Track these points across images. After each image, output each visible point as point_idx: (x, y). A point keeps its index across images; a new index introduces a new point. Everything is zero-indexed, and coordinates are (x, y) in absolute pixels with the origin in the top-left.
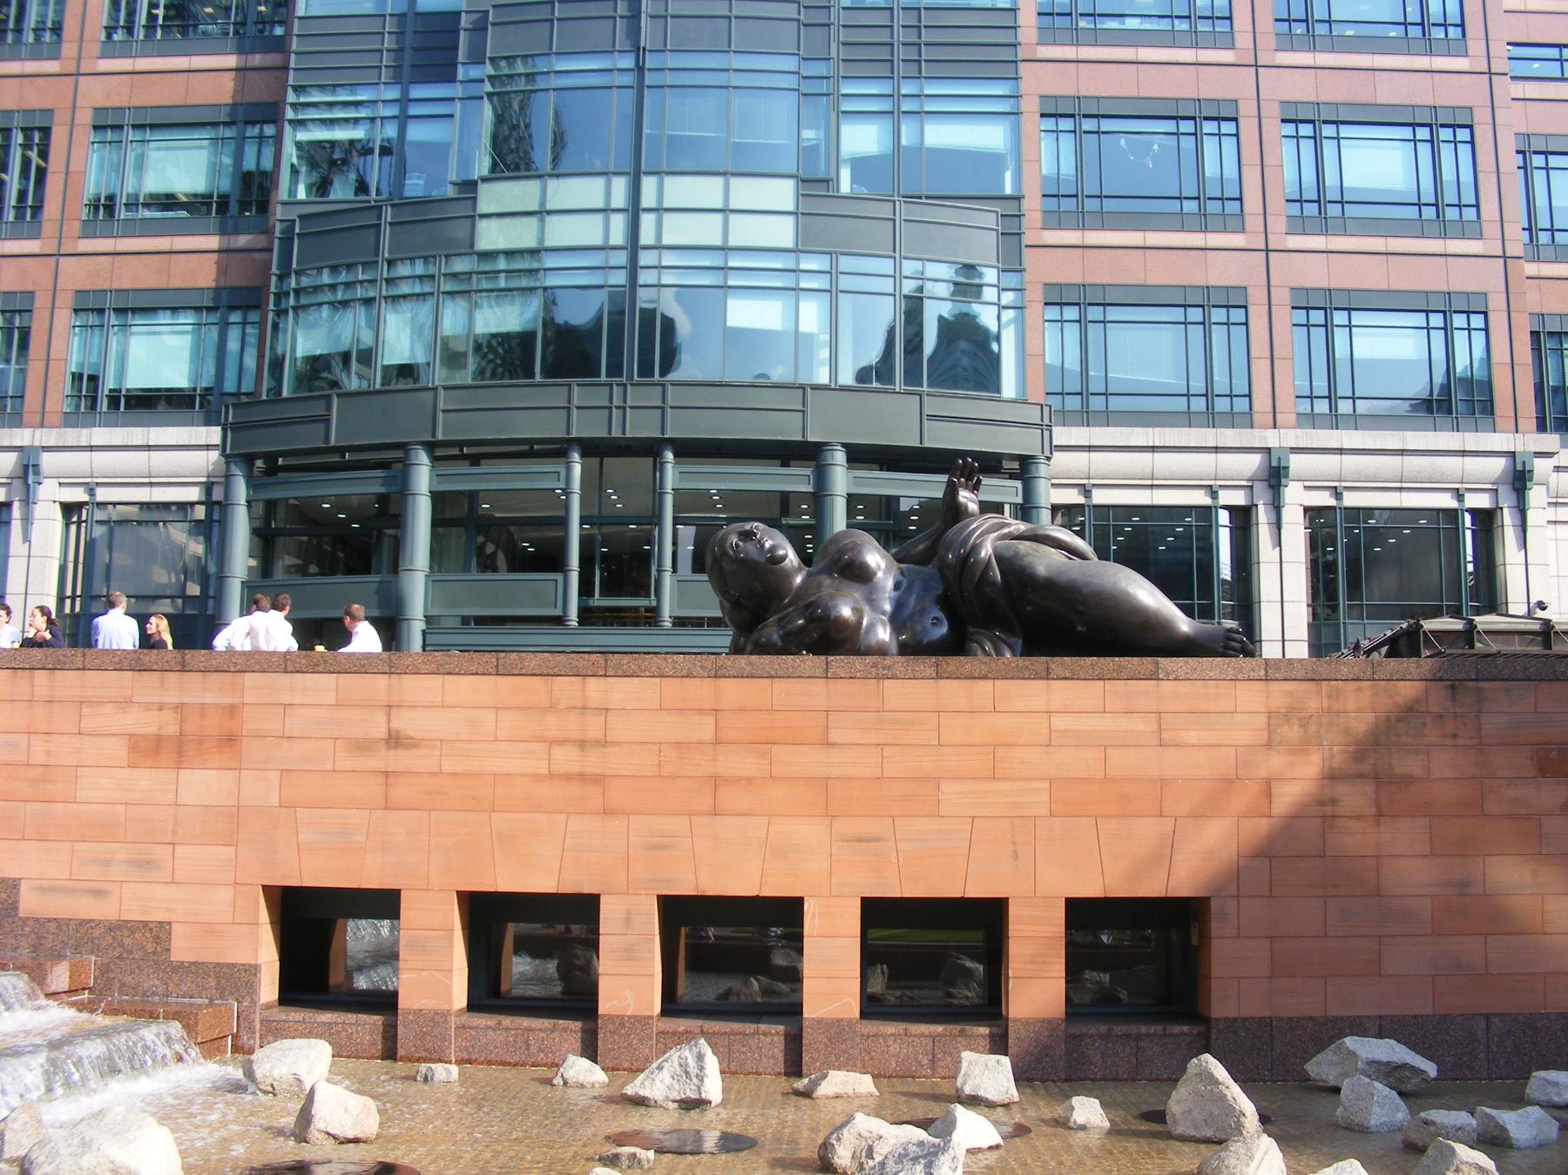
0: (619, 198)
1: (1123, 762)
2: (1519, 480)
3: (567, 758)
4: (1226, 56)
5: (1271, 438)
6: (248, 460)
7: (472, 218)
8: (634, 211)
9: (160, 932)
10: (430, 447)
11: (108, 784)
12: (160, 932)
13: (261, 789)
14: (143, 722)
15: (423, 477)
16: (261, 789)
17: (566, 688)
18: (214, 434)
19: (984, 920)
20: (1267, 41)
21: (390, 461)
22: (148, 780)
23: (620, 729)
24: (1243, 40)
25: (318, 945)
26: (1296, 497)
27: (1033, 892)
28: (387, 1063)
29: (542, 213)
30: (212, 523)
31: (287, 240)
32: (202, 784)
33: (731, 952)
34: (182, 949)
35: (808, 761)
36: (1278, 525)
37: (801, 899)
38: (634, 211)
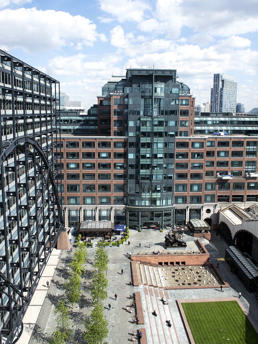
11: (154, 259)
32: (156, 259)
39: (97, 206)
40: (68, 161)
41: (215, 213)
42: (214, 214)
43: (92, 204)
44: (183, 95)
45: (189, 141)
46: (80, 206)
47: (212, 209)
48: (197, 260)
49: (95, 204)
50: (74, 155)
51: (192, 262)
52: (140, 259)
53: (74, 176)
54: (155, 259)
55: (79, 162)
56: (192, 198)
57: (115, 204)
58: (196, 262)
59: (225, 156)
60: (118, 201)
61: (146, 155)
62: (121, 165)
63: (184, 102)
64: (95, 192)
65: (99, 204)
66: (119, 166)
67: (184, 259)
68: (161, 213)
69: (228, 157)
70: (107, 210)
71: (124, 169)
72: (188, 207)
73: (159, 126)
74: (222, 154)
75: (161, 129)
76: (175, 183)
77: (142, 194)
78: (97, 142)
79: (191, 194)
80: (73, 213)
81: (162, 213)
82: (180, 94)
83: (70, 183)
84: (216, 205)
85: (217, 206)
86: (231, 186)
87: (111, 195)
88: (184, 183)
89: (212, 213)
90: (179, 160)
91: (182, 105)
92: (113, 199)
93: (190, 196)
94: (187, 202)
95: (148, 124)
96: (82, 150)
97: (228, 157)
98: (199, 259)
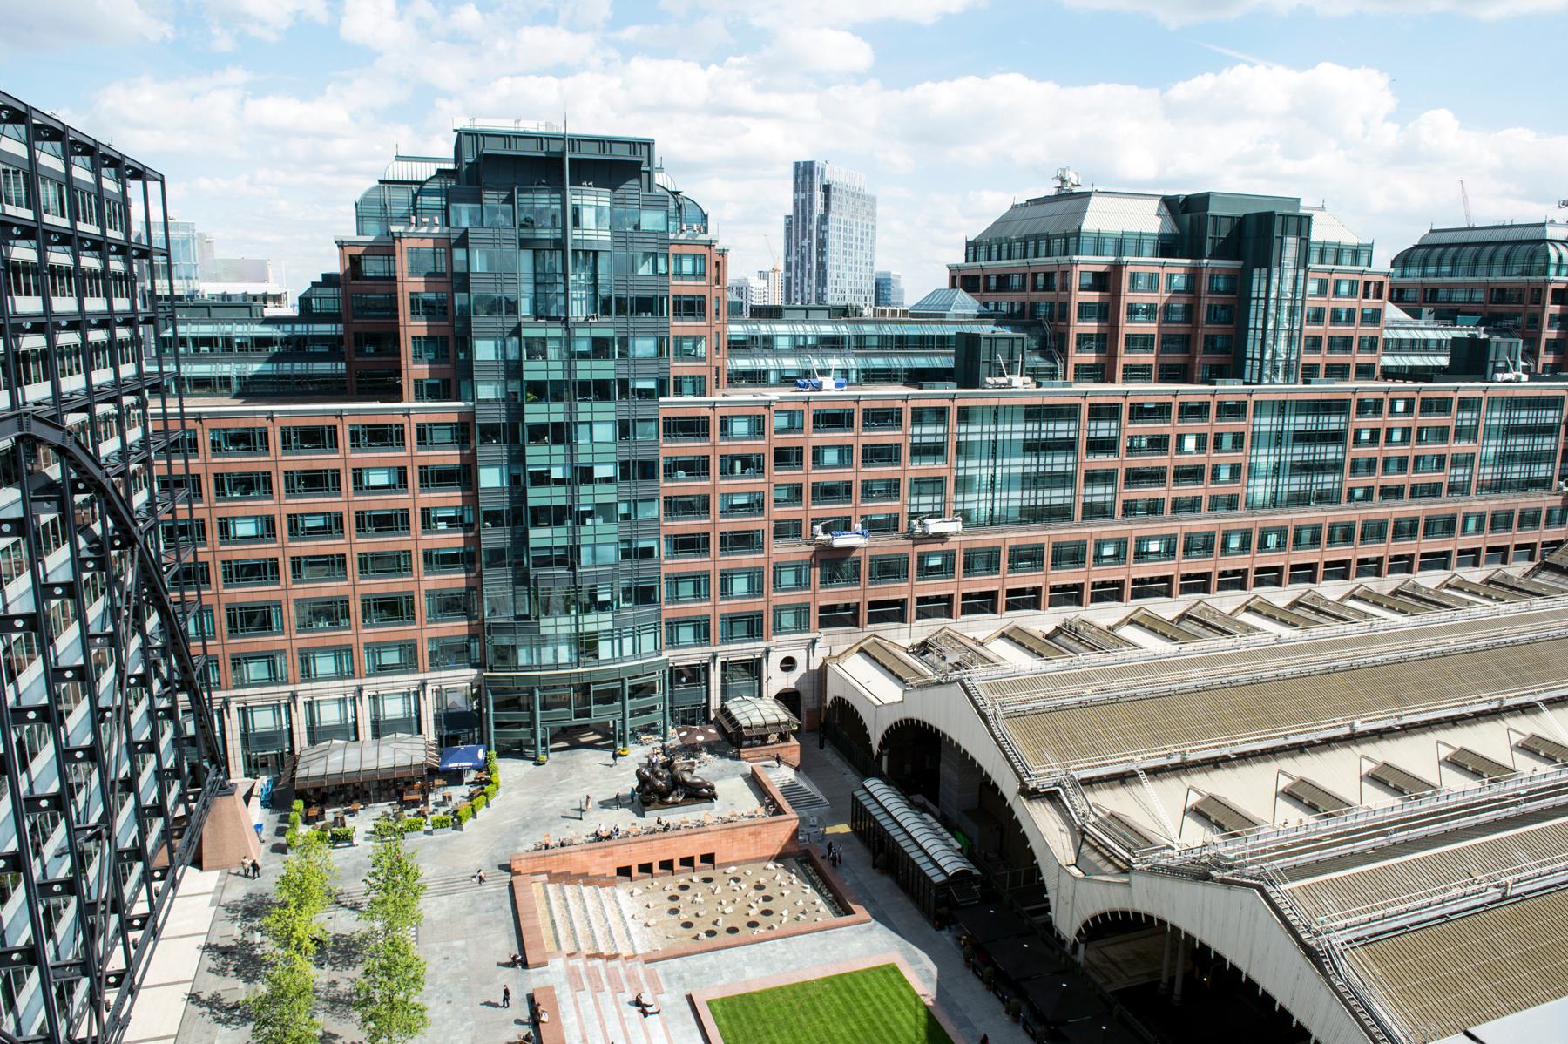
11: (598, 860)
32: (609, 859)
39: (364, 681)
43: (340, 676)
47: (800, 656)
56: (730, 621)
57: (435, 666)
60: (448, 654)
61: (549, 472)
62: (451, 513)
64: (349, 628)
65: (369, 676)
70: (406, 695)
72: (714, 657)
73: (597, 357)
74: (831, 457)
77: (543, 622)
79: (726, 606)
83: (240, 599)
89: (801, 669)
96: (279, 461)
98: (764, 836)
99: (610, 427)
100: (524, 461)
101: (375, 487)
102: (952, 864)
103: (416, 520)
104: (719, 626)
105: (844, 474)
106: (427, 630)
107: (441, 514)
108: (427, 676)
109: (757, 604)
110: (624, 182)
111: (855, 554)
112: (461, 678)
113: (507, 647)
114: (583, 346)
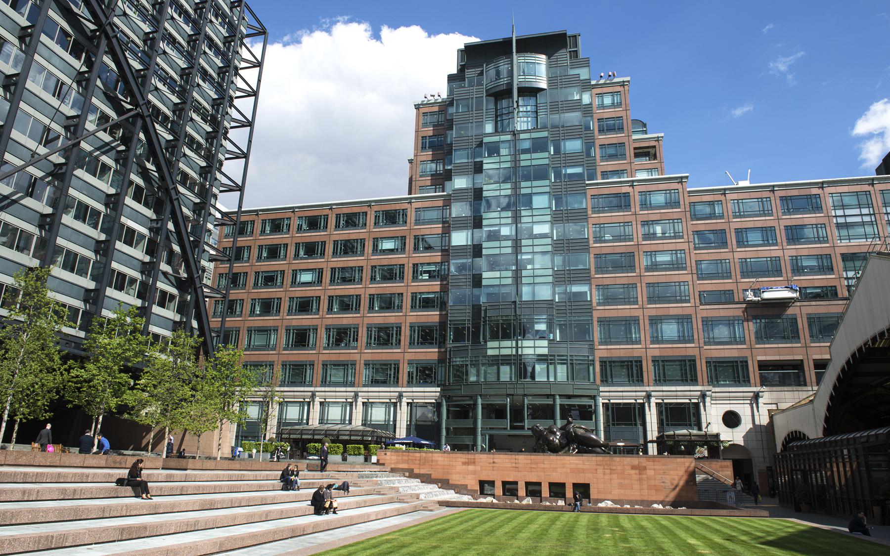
0: (514, 345)
1: (579, 466)
2: (703, 396)
3: (514, 465)
4: (636, 306)
5: (647, 389)
6: (445, 397)
7: (486, 349)
8: (517, 347)
9: (467, 486)
10: (481, 395)
11: (460, 467)
12: (467, 486)
13: (478, 468)
14: (464, 460)
15: (480, 401)
16: (478, 468)
17: (514, 457)
18: (439, 389)
19: (563, 485)
20: (645, 303)
21: (473, 398)
22: (464, 467)
23: (520, 461)
24: (640, 303)
25: (485, 486)
26: (653, 401)
27: (569, 481)
28: (886, 136)
29: (499, 348)
30: (438, 406)
31: (450, 351)
32: (471, 468)
33: (533, 489)
34: (469, 488)
35: (542, 465)
36: (649, 407)
37: (588, 485)
38: (517, 347)
39: (359, 389)
40: (298, 264)
41: (757, 423)
42: (757, 429)
43: (345, 384)
44: (602, 81)
45: (630, 190)
46: (312, 389)
47: (743, 410)
48: (640, 480)
49: (352, 385)
50: (311, 249)
51: (621, 486)
52: (407, 462)
53: (305, 306)
54: (465, 463)
55: (323, 266)
56: (660, 363)
57: (410, 383)
58: (636, 486)
59: (766, 242)
60: (424, 374)
61: (499, 231)
62: (433, 268)
63: (608, 100)
64: (356, 348)
65: (364, 386)
66: (425, 272)
67: (583, 471)
68: (550, 402)
69: (776, 245)
70: (387, 405)
71: (441, 281)
72: (648, 396)
73: (535, 151)
74: (754, 238)
75: (541, 159)
76: (596, 315)
77: (490, 344)
78: (373, 212)
79: (655, 350)
80: (293, 413)
81: (554, 401)
82: (593, 82)
83: (294, 323)
84: (756, 396)
85: (761, 400)
86: (800, 326)
87: (399, 357)
88: (627, 314)
89: (746, 425)
90: (603, 245)
91: (602, 106)
92: (405, 370)
93: (655, 361)
94: (645, 380)
95: (504, 151)
96: (364, 289)
97: (774, 245)
98: (650, 473)
99: (546, 197)
100: (580, 413)
101: (384, 251)
102: (751, 108)
103: (408, 272)
104: (651, 368)
105: (774, 251)
106: (408, 354)
107: (426, 268)
108: (404, 389)
109: (688, 349)
110: (556, 51)
111: (790, 311)
112: (430, 393)
113: (462, 366)
114: (527, 145)
